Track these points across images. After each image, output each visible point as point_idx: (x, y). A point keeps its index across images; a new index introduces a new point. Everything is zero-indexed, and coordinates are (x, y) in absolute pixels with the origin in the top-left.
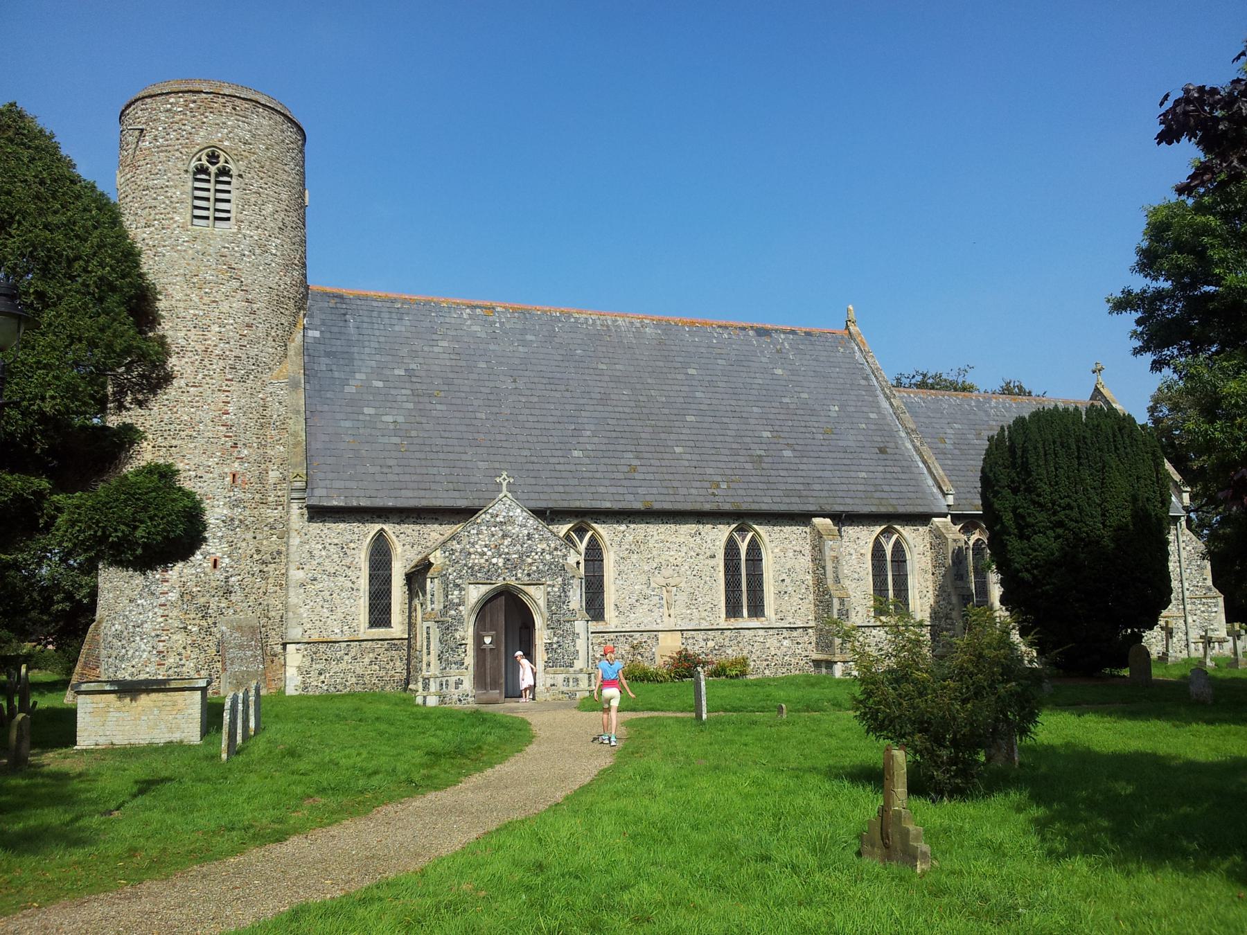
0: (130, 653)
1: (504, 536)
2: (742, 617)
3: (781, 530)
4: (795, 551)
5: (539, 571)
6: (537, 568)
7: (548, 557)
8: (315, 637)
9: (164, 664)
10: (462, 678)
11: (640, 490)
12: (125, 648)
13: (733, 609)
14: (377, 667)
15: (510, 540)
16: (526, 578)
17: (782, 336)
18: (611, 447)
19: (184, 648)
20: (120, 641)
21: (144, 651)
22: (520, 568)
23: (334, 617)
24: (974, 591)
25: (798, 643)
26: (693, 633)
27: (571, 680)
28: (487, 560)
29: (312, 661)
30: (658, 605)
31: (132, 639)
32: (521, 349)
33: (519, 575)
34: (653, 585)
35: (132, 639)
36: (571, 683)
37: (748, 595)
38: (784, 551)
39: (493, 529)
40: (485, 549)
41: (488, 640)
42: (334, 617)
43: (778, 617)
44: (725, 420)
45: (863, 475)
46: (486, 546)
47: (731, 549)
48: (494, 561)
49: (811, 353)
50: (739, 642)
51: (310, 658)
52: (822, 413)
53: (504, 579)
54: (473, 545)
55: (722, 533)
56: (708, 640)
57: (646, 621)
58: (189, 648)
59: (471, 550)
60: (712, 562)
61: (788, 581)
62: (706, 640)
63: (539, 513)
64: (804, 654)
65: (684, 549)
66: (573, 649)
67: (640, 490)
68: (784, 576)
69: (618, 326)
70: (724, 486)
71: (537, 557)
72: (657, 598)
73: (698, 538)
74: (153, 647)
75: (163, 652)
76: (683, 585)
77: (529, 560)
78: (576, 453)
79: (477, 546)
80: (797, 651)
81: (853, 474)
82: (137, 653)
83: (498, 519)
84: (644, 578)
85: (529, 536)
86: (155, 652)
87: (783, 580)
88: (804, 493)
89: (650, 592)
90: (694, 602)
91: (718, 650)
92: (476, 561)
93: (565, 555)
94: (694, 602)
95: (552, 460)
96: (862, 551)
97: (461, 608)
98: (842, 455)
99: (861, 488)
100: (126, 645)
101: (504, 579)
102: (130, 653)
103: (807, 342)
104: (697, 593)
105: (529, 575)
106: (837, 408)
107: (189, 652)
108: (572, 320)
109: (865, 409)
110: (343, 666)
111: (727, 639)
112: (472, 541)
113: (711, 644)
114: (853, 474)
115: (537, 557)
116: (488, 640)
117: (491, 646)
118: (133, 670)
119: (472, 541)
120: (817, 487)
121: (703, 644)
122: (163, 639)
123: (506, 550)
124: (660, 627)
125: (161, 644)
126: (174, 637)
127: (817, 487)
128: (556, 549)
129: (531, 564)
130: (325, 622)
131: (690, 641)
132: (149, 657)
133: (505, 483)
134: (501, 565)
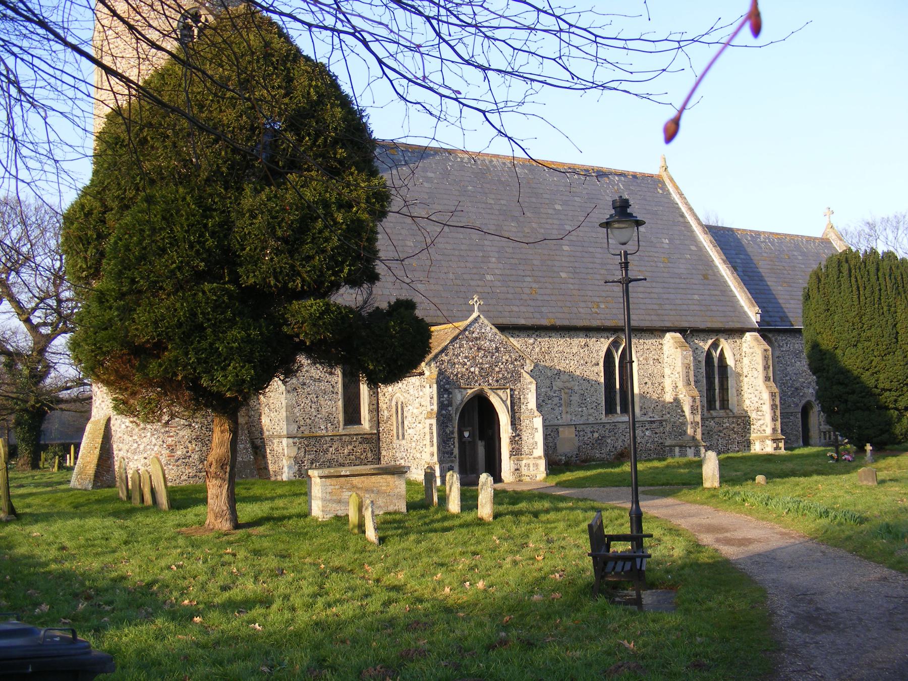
0: (142, 447)
1: (479, 349)
2: (616, 412)
3: (586, 345)
4: (654, 359)
5: (505, 378)
6: (503, 375)
7: (511, 366)
8: (307, 433)
9: (174, 456)
10: (453, 465)
11: (543, 309)
12: (137, 442)
13: (610, 409)
14: (354, 457)
15: (483, 352)
16: (496, 384)
17: (617, 178)
18: (513, 272)
19: (190, 442)
20: (131, 436)
21: (155, 445)
22: (491, 375)
23: (319, 416)
24: (618, 386)
25: (656, 433)
26: (583, 426)
27: (531, 466)
28: (467, 369)
29: (305, 452)
30: (558, 405)
31: (143, 435)
32: (426, 184)
33: (490, 381)
34: (555, 388)
35: (143, 435)
36: (531, 468)
37: (620, 395)
38: (646, 359)
39: (471, 343)
40: (466, 360)
41: (466, 434)
42: (319, 416)
43: (642, 412)
44: (591, 250)
45: (696, 297)
46: (466, 357)
47: (609, 357)
48: (472, 369)
49: (640, 193)
50: (615, 434)
51: (303, 450)
52: (658, 245)
53: (480, 385)
54: (458, 356)
55: (601, 345)
56: (594, 432)
57: (549, 418)
58: (194, 442)
59: (456, 360)
60: (596, 369)
61: (649, 383)
62: (593, 432)
63: (502, 328)
64: (660, 441)
65: (577, 358)
66: (531, 441)
67: (543, 309)
68: (646, 380)
69: (495, 167)
70: (603, 306)
71: (502, 366)
72: (558, 398)
73: (586, 349)
74: (163, 441)
75: (172, 446)
76: (576, 388)
77: (497, 369)
78: (489, 277)
79: (460, 358)
80: (656, 439)
81: (689, 297)
82: (149, 447)
83: (474, 335)
84: (548, 382)
85: (497, 349)
86: (165, 446)
87: (646, 383)
88: (660, 312)
89: (552, 394)
90: (584, 402)
91: (601, 440)
92: (459, 370)
93: (523, 365)
94: (584, 402)
95: (473, 283)
96: (700, 359)
97: (450, 408)
98: (678, 281)
99: (697, 308)
100: (138, 440)
101: (480, 385)
102: (142, 447)
103: (634, 184)
104: (586, 394)
105: (497, 381)
106: (667, 241)
107: (194, 446)
108: (459, 159)
109: (686, 242)
110: (329, 456)
111: (607, 431)
112: (456, 353)
113: (596, 435)
114: (689, 297)
115: (502, 366)
116: (466, 434)
117: (469, 439)
118: (146, 461)
119: (456, 353)
120: (667, 307)
121: (590, 435)
122: (171, 434)
123: (481, 361)
124: (560, 422)
125: (170, 439)
126: (181, 433)
127: (667, 307)
128: (516, 360)
129: (498, 372)
130: (314, 420)
131: (581, 433)
132: (160, 449)
133: (476, 307)
134: (477, 373)
